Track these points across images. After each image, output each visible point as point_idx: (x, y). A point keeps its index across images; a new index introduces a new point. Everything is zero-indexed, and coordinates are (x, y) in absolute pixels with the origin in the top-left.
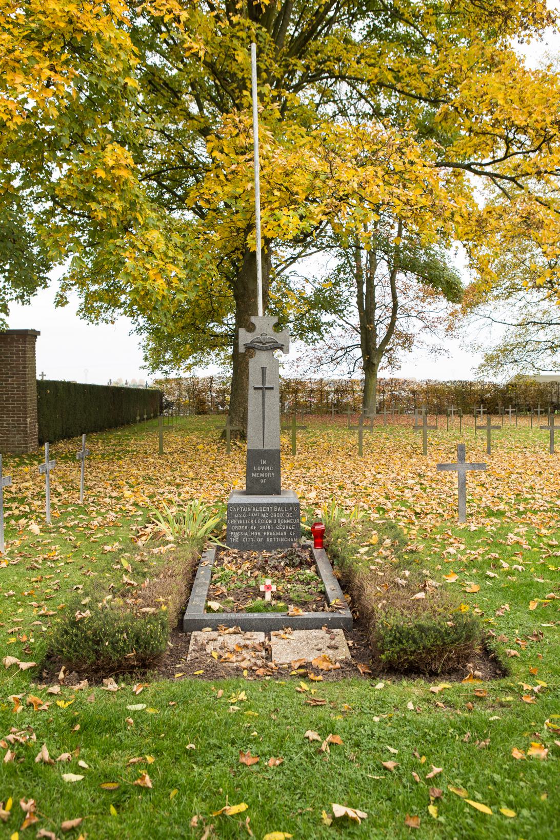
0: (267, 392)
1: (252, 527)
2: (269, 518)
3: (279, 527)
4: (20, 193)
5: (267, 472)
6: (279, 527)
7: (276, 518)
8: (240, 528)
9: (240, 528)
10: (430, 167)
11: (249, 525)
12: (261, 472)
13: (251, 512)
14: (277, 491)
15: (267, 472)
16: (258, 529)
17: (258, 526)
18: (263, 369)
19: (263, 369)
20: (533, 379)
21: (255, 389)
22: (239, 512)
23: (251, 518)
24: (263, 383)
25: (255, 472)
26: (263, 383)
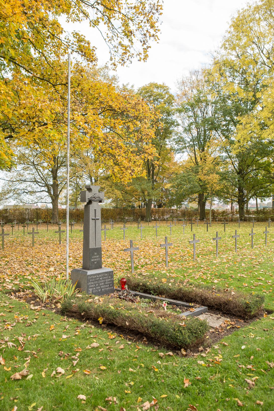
0: (97, 221)
1: (97, 285)
2: (103, 279)
3: (106, 283)
4: (160, 131)
5: (97, 258)
6: (106, 283)
7: (105, 279)
8: (92, 286)
9: (92, 286)
10: (255, 170)
11: (95, 284)
12: (95, 258)
13: (96, 278)
14: (100, 267)
15: (97, 258)
16: (99, 286)
17: (99, 284)
18: (95, 210)
19: (95, 210)
20: (22, 207)
21: (92, 219)
22: (92, 279)
23: (96, 281)
24: (95, 217)
25: (92, 259)
26: (95, 217)
